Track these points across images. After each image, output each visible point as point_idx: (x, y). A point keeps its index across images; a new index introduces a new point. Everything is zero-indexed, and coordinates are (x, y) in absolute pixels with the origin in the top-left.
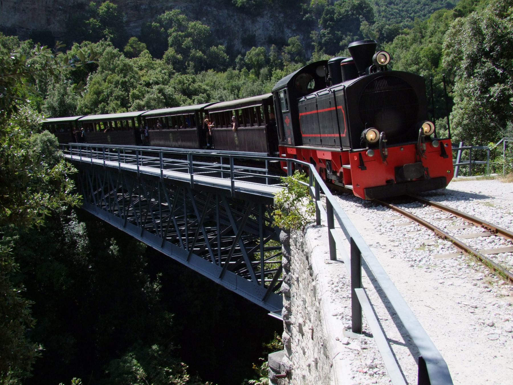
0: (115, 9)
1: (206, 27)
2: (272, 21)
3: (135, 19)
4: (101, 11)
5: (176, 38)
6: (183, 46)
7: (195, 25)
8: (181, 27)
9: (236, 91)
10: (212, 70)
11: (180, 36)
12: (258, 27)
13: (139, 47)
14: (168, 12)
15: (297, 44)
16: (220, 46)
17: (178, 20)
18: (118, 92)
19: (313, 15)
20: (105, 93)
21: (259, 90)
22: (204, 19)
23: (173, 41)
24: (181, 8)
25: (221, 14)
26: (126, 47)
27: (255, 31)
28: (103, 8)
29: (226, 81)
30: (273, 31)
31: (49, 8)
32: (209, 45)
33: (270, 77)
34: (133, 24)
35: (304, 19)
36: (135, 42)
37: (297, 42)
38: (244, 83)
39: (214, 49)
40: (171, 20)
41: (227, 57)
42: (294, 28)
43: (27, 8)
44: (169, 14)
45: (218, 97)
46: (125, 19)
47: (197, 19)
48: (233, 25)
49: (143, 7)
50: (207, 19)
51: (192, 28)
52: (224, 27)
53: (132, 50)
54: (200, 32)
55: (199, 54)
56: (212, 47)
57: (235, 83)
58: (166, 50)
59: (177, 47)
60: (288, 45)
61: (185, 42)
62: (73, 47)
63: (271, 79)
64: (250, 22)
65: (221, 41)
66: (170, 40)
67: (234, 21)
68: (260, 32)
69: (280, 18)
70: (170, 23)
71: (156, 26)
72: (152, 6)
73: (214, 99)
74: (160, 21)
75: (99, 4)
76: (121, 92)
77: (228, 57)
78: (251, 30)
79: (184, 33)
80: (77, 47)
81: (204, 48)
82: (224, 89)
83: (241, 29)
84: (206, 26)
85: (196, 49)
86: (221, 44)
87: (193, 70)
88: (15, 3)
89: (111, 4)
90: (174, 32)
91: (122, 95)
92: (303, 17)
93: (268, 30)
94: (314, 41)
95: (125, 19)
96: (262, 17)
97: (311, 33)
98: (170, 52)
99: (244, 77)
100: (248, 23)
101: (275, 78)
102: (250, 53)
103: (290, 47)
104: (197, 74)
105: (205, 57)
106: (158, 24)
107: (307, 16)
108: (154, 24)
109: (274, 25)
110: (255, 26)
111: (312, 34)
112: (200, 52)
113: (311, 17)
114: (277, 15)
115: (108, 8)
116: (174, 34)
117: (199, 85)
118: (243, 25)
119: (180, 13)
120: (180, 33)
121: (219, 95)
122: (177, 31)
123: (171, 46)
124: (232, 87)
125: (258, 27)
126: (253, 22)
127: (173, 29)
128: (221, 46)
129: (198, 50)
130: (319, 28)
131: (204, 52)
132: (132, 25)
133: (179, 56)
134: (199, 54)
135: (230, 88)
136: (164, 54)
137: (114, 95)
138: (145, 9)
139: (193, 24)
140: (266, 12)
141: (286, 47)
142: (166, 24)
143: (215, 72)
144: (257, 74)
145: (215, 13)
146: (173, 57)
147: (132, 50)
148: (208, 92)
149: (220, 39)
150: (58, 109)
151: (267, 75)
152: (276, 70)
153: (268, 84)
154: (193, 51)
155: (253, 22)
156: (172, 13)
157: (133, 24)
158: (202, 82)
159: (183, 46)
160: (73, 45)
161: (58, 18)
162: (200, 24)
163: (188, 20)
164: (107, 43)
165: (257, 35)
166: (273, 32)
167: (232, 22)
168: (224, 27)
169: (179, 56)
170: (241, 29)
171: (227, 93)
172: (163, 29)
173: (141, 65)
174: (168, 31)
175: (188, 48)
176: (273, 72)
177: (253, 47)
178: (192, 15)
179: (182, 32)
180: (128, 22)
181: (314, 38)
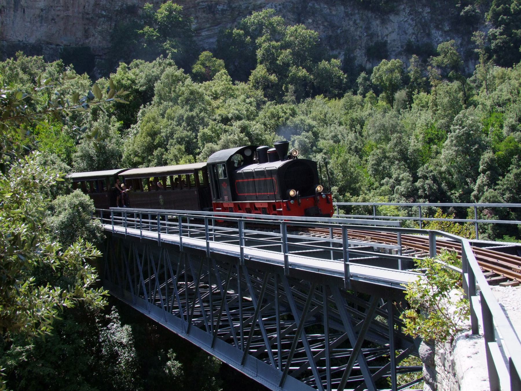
0: (180, 12)
1: (312, 33)
2: (412, 19)
3: (208, 25)
4: (159, 16)
5: (267, 50)
6: (278, 62)
7: (296, 30)
8: (275, 35)
9: (358, 127)
10: (322, 95)
11: (274, 47)
12: (390, 29)
13: (214, 66)
14: (257, 14)
15: (451, 53)
16: (333, 61)
17: (271, 24)
18: (182, 132)
19: (476, 6)
20: (163, 134)
21: (392, 125)
22: (310, 21)
23: (263, 54)
24: (276, 7)
25: (334, 13)
26: (195, 66)
27: (387, 35)
28: (162, 12)
29: (343, 112)
30: (413, 34)
31: (88, 14)
32: (317, 59)
33: (410, 104)
34: (207, 33)
35: (462, 13)
36: (208, 59)
37: (451, 49)
38: (370, 115)
39: (324, 64)
40: (260, 25)
41: (344, 77)
42: (447, 28)
43: (58, 16)
44: (257, 16)
45: (330, 136)
46: (194, 26)
47: (299, 21)
48: (352, 29)
49: (220, 7)
50: (313, 21)
51: (291, 36)
52: (339, 31)
53: (203, 70)
54: (303, 41)
55: (303, 72)
56: (321, 61)
57: (356, 114)
58: (254, 68)
59: (270, 63)
60: (437, 54)
61: (282, 56)
62: (119, 69)
63: (411, 107)
64: (378, 22)
65: (335, 53)
66: (259, 53)
67: (355, 22)
68: (394, 36)
69: (426, 15)
70: (258, 31)
71: (238, 34)
72: (233, 6)
73: (325, 139)
74: (244, 27)
75: (157, 6)
76: (185, 132)
77: (346, 76)
78: (380, 34)
79: (279, 43)
80: (124, 69)
81: (309, 63)
82: (340, 124)
83: (365, 34)
84: (313, 32)
85: (298, 66)
86: (336, 57)
87: (293, 98)
88: (42, 10)
89: (175, 6)
90: (264, 41)
91: (187, 136)
92: (461, 11)
93: (406, 34)
94: (477, 47)
95: (194, 26)
96: (397, 13)
97: (472, 35)
98: (260, 71)
99: (369, 105)
100: (376, 25)
101: (418, 105)
102: (379, 70)
103: (440, 58)
104: (299, 102)
105: (312, 77)
106: (242, 32)
107: (467, 8)
108: (235, 31)
109: (416, 26)
110: (387, 28)
111: (475, 36)
112: (304, 71)
113: (474, 11)
114: (420, 10)
115: (170, 10)
116: (266, 45)
117: (302, 120)
118: (368, 28)
119: (275, 15)
120: (274, 43)
121: (333, 134)
122: (269, 40)
123: (261, 63)
124: (353, 120)
125: (390, 29)
126: (384, 22)
127: (264, 38)
128: (335, 60)
129: (301, 68)
130: (486, 26)
131: (309, 70)
132: (203, 34)
133: (273, 77)
134: (303, 72)
135: (348, 123)
136: (250, 74)
137: (175, 136)
138: (223, 10)
139: (293, 28)
140: (403, 7)
141: (435, 58)
142: (253, 30)
143: (327, 99)
144: (390, 100)
145: (326, 11)
146: (264, 78)
147: (203, 70)
148: (315, 129)
149: (332, 49)
150: (95, 158)
151: (405, 101)
152: (418, 93)
153: (407, 115)
154: (293, 69)
155: (384, 22)
156: (262, 14)
157: (207, 33)
158: (307, 115)
159: (278, 62)
160: (118, 66)
161: (100, 28)
162: (303, 29)
163: (286, 24)
164: (167, 62)
165: (389, 42)
166: (414, 36)
167: (351, 23)
168: (339, 31)
169: (273, 77)
170: (365, 34)
171: (345, 130)
172: (249, 37)
173: (216, 91)
174: (256, 41)
175: (287, 65)
176: (414, 97)
177: (384, 60)
178: (290, 16)
179: (277, 41)
180: (198, 30)
181: (478, 43)
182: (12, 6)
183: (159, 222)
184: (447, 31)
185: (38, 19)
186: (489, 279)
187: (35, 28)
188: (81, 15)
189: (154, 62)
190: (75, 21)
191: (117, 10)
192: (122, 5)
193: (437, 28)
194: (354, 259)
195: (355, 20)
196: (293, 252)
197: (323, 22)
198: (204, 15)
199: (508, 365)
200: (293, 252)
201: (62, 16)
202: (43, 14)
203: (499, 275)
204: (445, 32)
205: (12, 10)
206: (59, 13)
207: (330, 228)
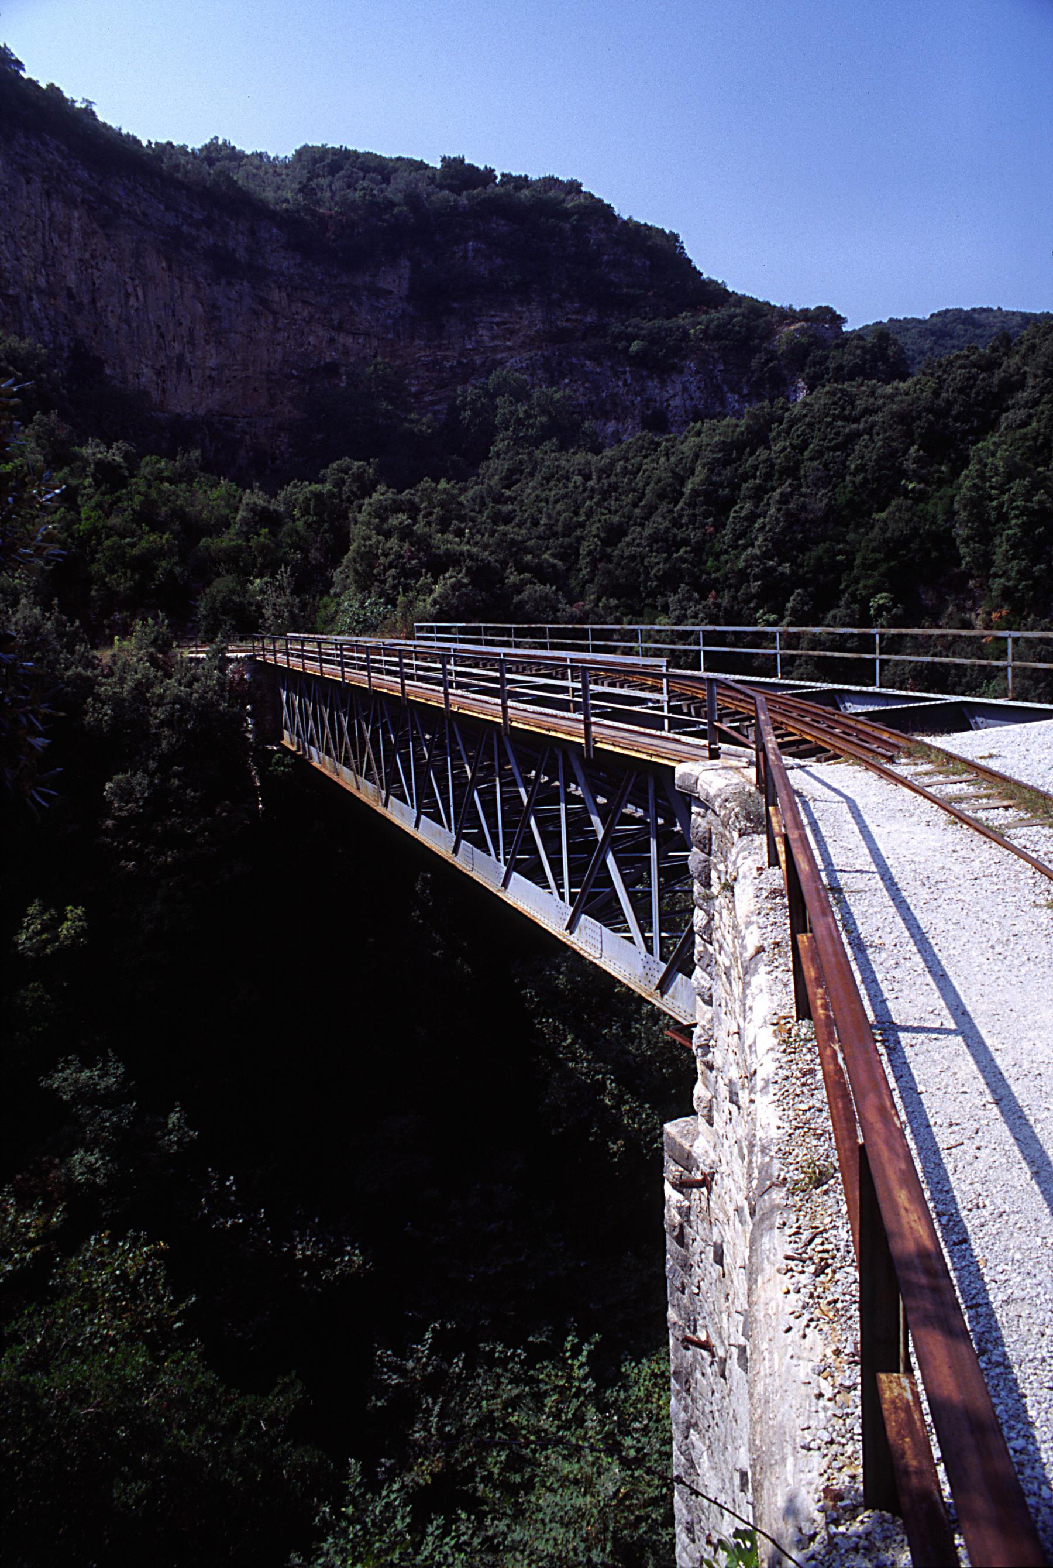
3: (432, 388)
68: (677, 402)
125: (671, 392)
126: (663, 383)
167: (620, 384)
182: (174, 365)
183: (502, 675)
184: (746, 395)
185: (208, 382)
186: (779, 740)
187: (204, 394)
188: (264, 376)
189: (619, 545)
190: (257, 385)
191: (312, 369)
192: (319, 362)
193: (733, 391)
194: (922, 704)
195: (626, 380)
196: (933, 703)
197: (583, 383)
198: (427, 374)
199: (990, 721)
200: (933, 703)
201: (239, 377)
202: (215, 373)
203: (793, 734)
204: (744, 396)
205: (174, 372)
206: (235, 374)
207: (665, 681)
